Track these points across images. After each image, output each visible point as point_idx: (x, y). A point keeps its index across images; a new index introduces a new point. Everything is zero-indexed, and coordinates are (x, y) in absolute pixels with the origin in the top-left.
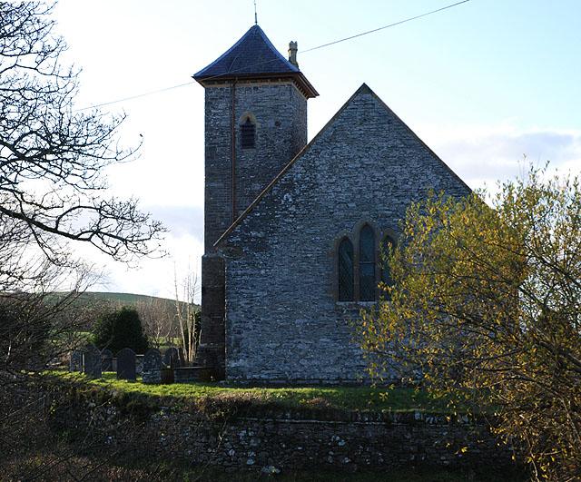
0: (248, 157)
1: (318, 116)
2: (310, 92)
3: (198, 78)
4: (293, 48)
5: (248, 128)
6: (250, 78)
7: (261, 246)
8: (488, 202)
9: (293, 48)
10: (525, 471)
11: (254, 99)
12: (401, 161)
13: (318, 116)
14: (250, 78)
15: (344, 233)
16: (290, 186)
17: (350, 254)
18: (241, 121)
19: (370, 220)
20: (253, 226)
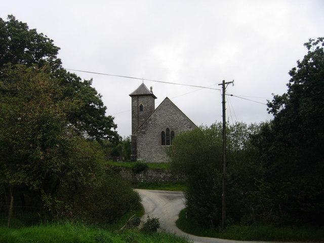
0: (141, 113)
1: (157, 103)
2: (155, 98)
3: (131, 95)
4: (151, 88)
5: (141, 106)
6: (142, 97)
7: (144, 133)
8: (183, 207)
9: (151, 88)
10: (319, 51)
11: (141, 101)
12: (175, 114)
13: (157, 103)
14: (142, 97)
15: (163, 130)
16: (150, 120)
17: (164, 135)
18: (140, 105)
19: (168, 127)
20: (142, 129)
